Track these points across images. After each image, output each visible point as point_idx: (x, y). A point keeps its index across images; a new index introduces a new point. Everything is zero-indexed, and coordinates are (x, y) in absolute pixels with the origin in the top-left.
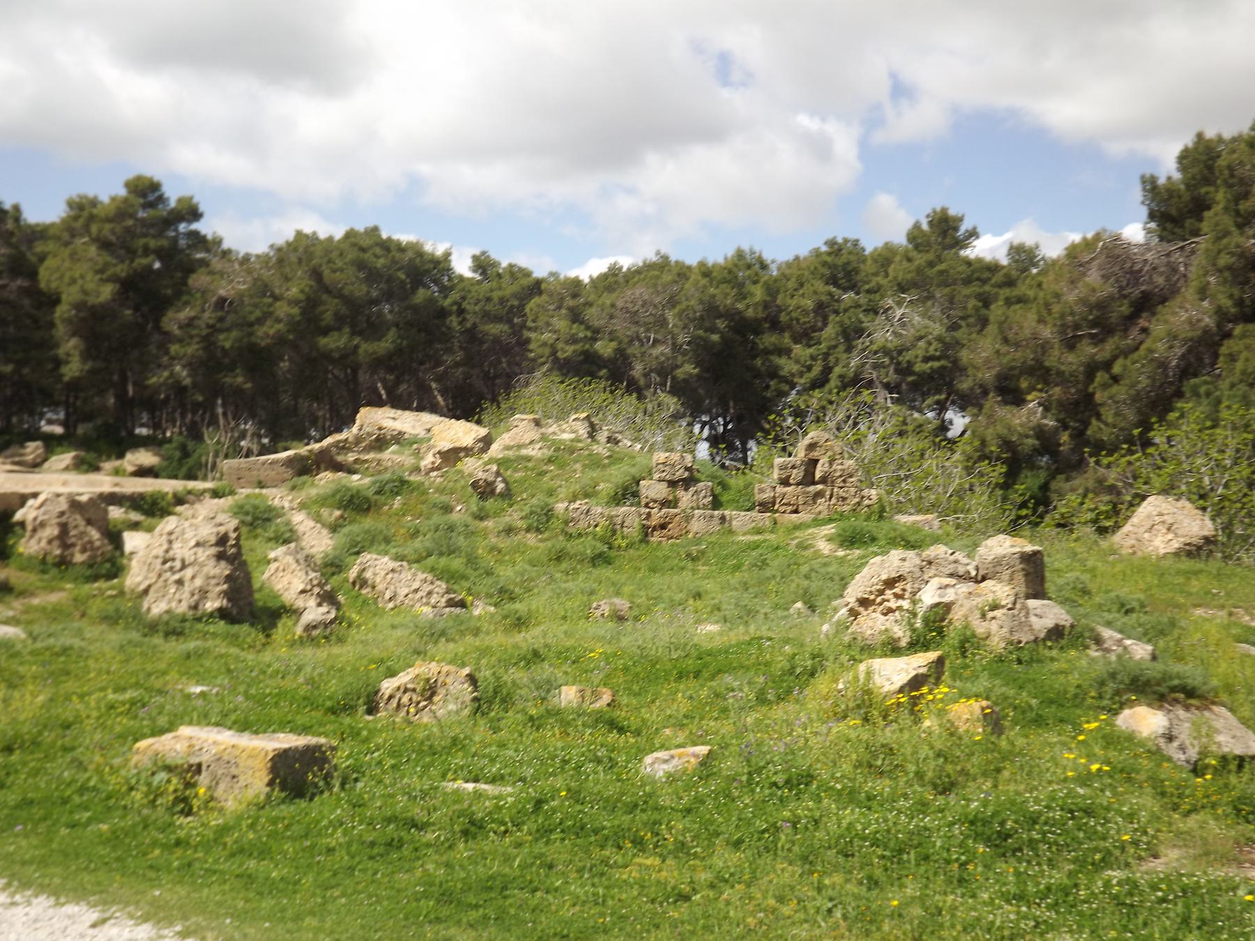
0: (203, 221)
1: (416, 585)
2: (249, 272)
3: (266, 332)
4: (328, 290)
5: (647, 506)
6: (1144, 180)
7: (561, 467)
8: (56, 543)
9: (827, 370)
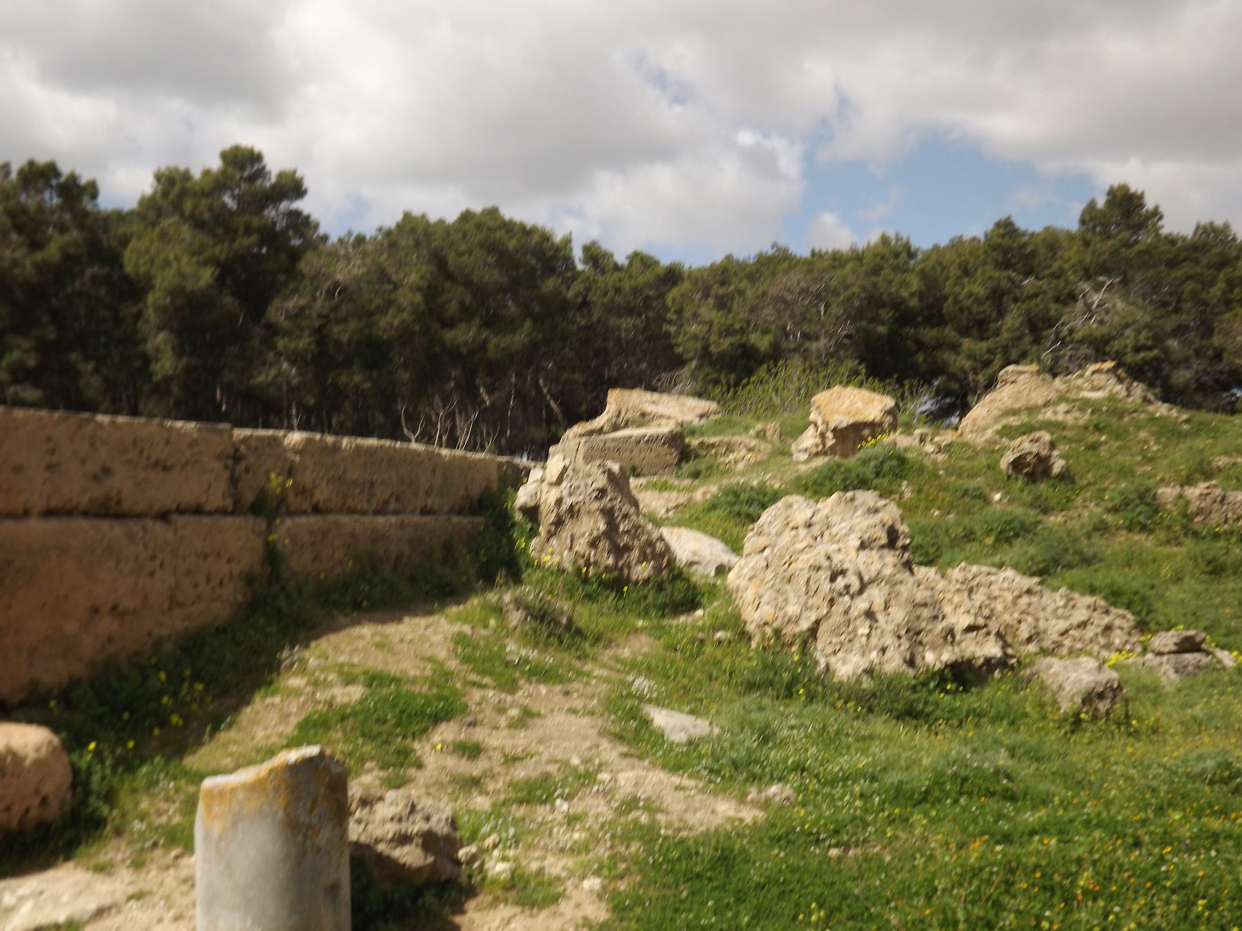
0: (307, 198)
1: (1080, 615)
2: (364, 254)
3: (389, 323)
4: (449, 276)
8: (604, 544)
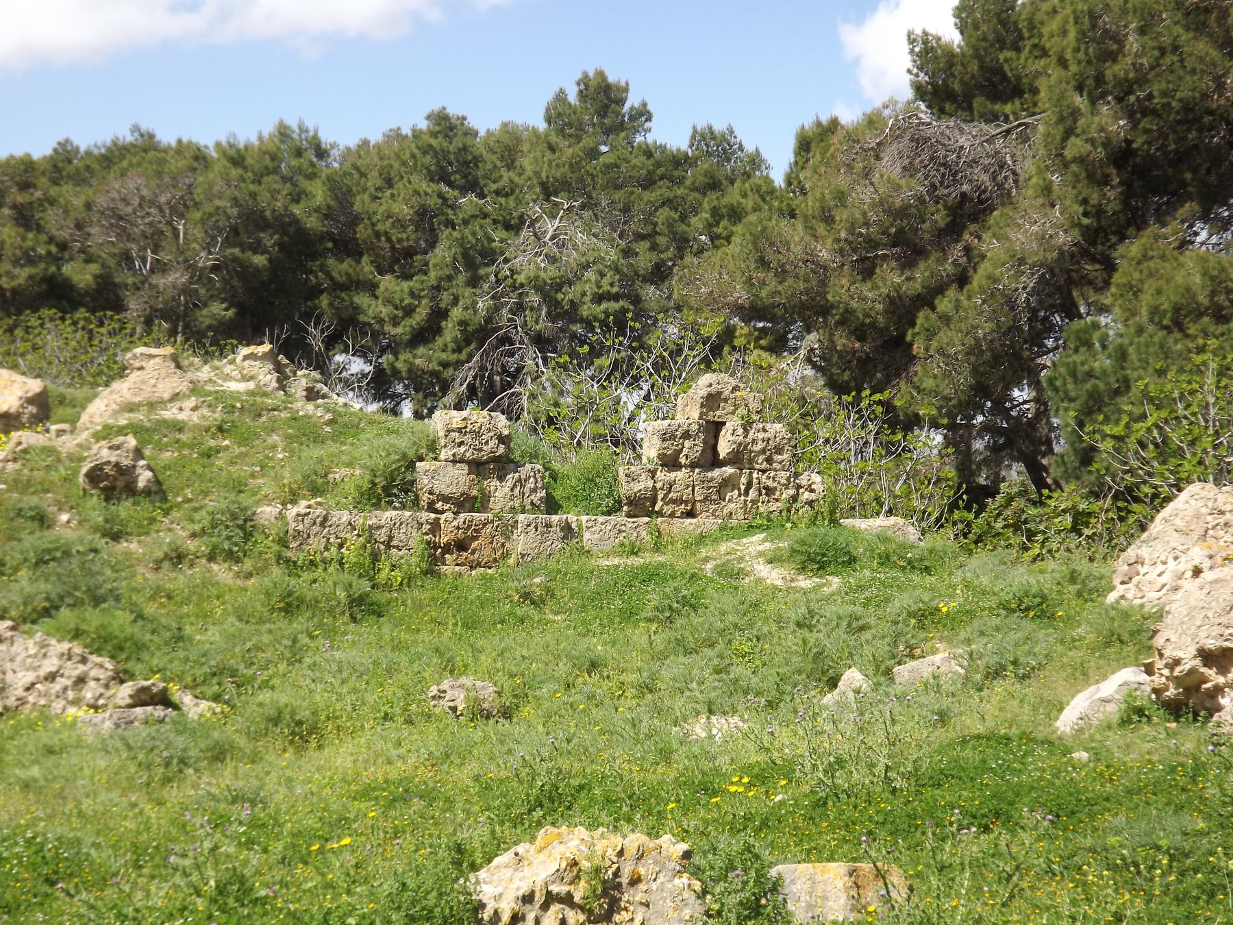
1: (50, 665)
5: (431, 508)
6: (912, 41)
7: (244, 441)
9: (439, 315)
